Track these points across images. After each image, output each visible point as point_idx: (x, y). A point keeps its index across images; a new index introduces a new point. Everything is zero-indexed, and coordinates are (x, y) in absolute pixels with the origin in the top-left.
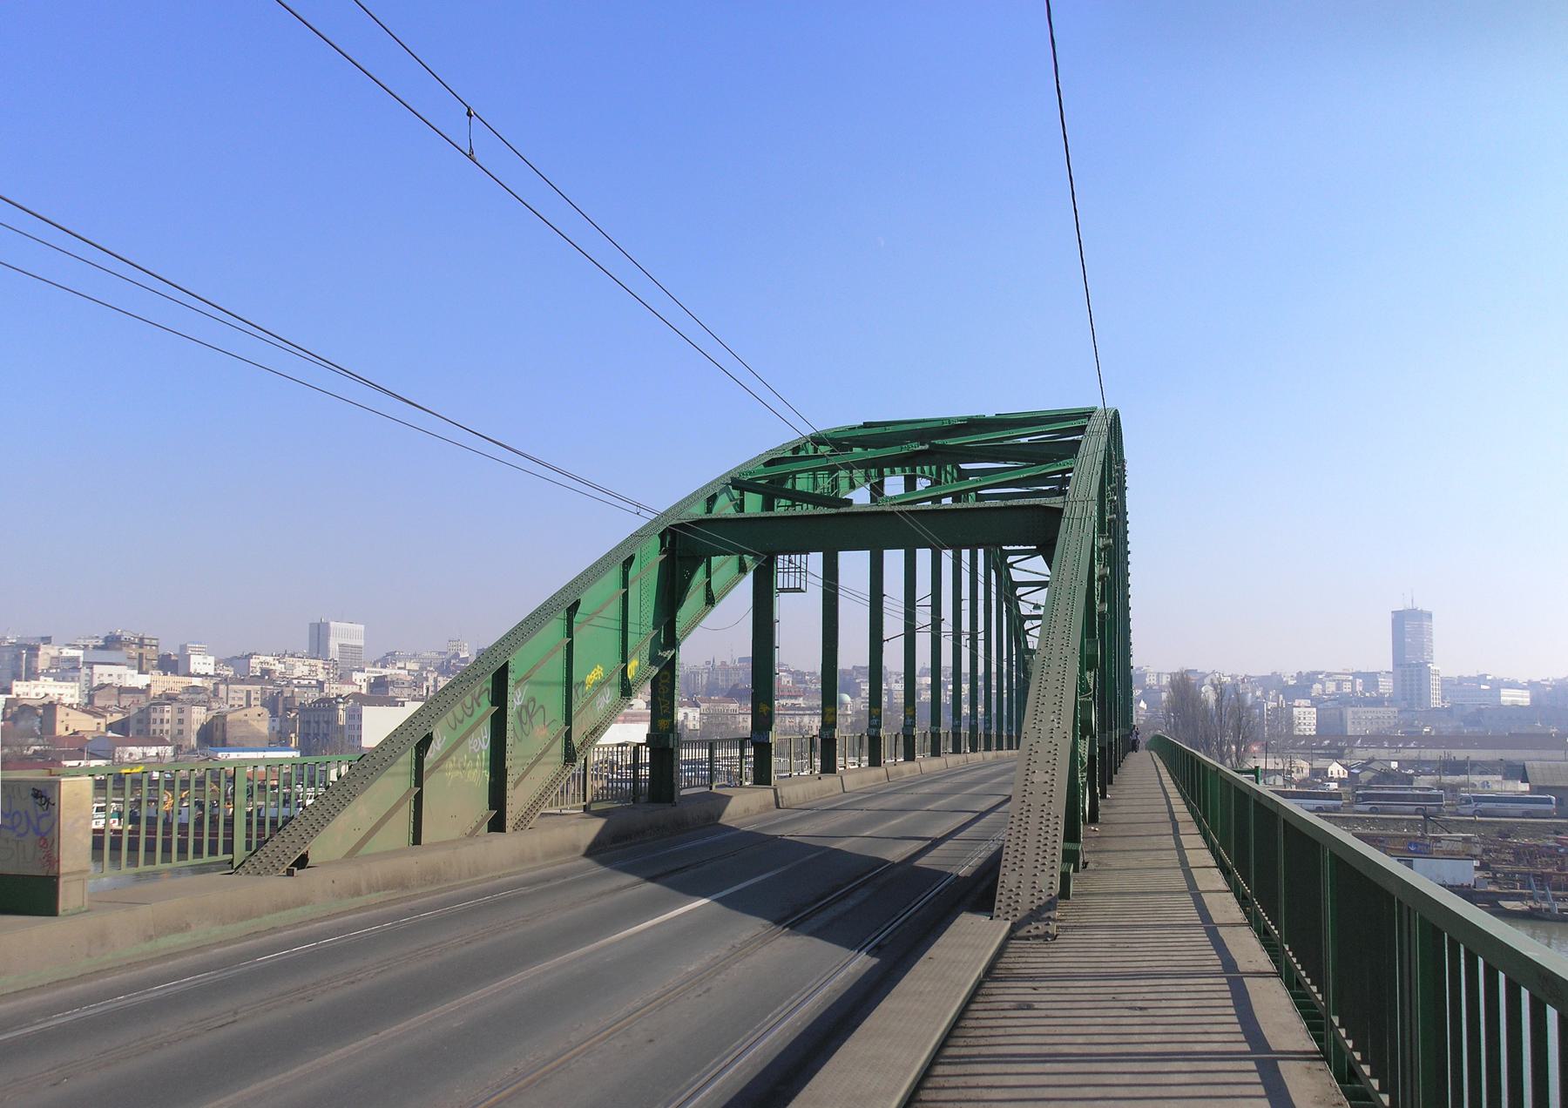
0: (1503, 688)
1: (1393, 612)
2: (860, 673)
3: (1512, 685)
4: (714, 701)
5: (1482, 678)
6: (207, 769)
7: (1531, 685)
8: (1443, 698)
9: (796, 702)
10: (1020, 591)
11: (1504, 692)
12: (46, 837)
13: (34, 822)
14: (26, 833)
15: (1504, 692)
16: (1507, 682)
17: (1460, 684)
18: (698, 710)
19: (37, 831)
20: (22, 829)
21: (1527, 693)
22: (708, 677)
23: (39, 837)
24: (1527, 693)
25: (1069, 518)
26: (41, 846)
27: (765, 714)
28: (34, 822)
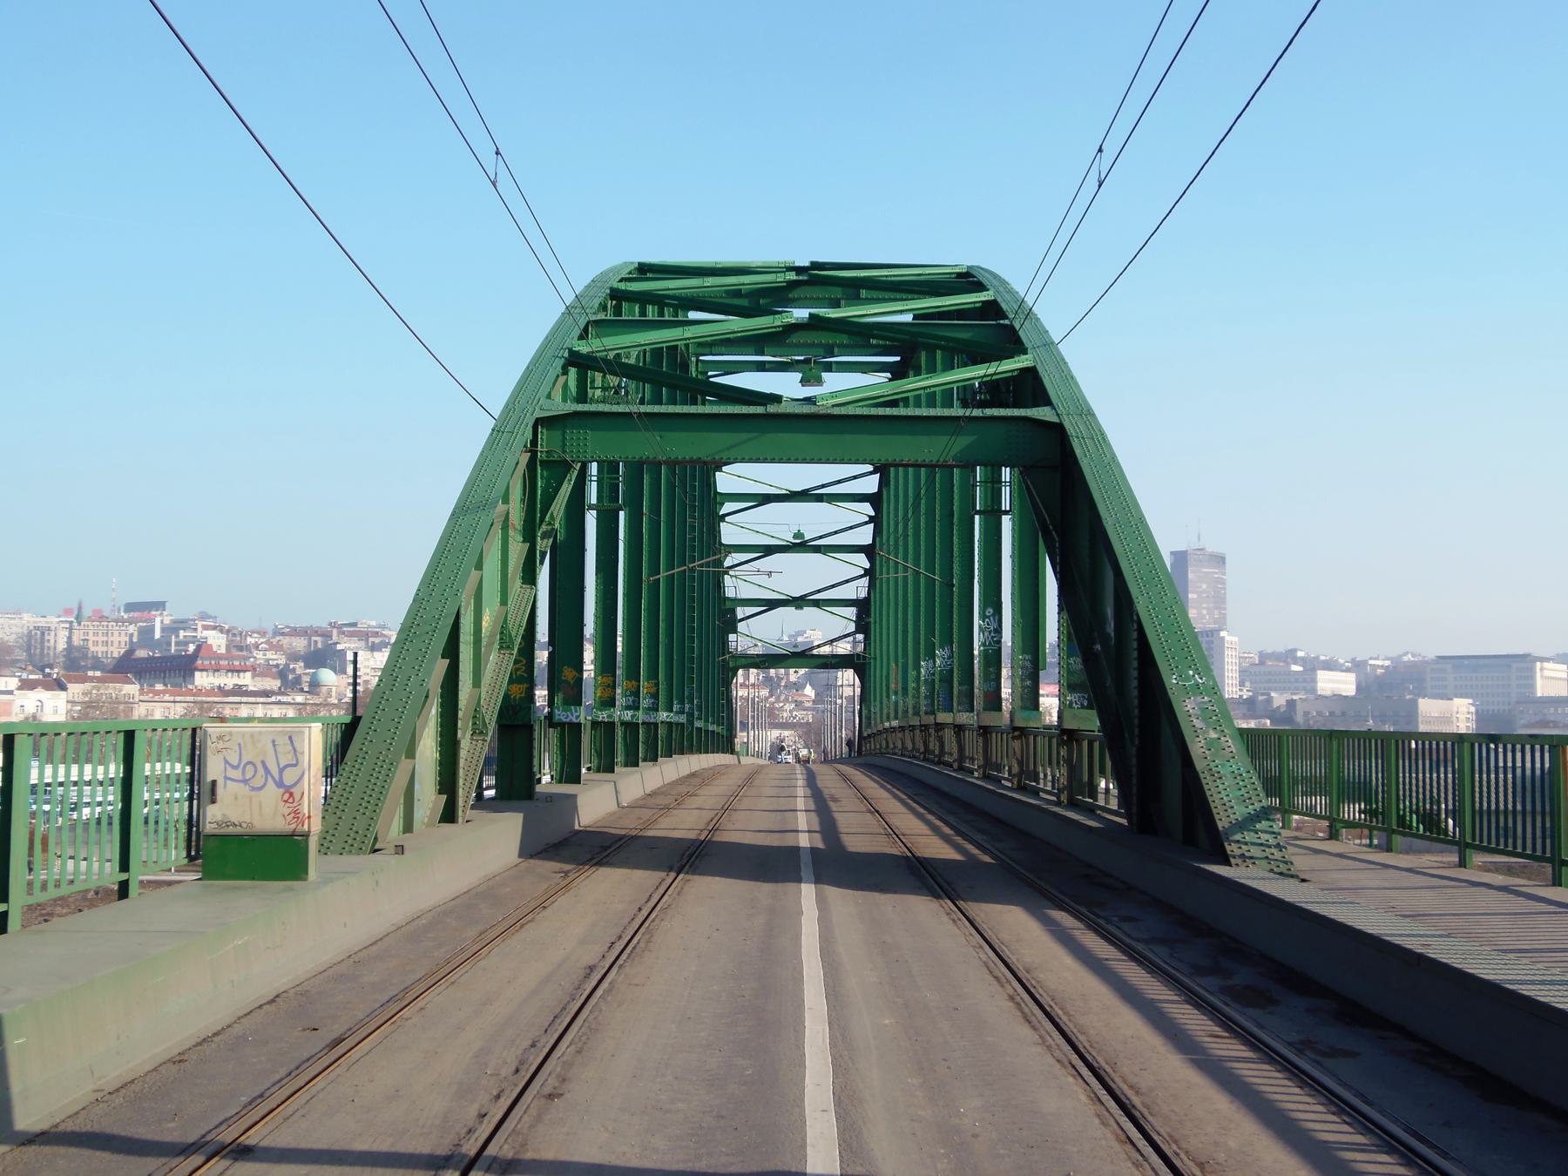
0: (1320, 669)
1: (1172, 553)
2: (343, 633)
3: (1330, 666)
4: (92, 679)
5: (1290, 656)
6: (69, 734)
7: (1357, 666)
8: (1242, 684)
9: (240, 682)
10: (728, 507)
11: (1322, 675)
12: (292, 790)
13: (275, 772)
14: (265, 784)
15: (1322, 675)
16: (1323, 661)
17: (1262, 663)
18: (63, 694)
19: (280, 784)
20: (258, 782)
21: (1352, 677)
22: (70, 638)
23: (282, 790)
24: (1352, 677)
25: (1078, 437)
26: (286, 801)
27: (572, 682)
28: (275, 772)
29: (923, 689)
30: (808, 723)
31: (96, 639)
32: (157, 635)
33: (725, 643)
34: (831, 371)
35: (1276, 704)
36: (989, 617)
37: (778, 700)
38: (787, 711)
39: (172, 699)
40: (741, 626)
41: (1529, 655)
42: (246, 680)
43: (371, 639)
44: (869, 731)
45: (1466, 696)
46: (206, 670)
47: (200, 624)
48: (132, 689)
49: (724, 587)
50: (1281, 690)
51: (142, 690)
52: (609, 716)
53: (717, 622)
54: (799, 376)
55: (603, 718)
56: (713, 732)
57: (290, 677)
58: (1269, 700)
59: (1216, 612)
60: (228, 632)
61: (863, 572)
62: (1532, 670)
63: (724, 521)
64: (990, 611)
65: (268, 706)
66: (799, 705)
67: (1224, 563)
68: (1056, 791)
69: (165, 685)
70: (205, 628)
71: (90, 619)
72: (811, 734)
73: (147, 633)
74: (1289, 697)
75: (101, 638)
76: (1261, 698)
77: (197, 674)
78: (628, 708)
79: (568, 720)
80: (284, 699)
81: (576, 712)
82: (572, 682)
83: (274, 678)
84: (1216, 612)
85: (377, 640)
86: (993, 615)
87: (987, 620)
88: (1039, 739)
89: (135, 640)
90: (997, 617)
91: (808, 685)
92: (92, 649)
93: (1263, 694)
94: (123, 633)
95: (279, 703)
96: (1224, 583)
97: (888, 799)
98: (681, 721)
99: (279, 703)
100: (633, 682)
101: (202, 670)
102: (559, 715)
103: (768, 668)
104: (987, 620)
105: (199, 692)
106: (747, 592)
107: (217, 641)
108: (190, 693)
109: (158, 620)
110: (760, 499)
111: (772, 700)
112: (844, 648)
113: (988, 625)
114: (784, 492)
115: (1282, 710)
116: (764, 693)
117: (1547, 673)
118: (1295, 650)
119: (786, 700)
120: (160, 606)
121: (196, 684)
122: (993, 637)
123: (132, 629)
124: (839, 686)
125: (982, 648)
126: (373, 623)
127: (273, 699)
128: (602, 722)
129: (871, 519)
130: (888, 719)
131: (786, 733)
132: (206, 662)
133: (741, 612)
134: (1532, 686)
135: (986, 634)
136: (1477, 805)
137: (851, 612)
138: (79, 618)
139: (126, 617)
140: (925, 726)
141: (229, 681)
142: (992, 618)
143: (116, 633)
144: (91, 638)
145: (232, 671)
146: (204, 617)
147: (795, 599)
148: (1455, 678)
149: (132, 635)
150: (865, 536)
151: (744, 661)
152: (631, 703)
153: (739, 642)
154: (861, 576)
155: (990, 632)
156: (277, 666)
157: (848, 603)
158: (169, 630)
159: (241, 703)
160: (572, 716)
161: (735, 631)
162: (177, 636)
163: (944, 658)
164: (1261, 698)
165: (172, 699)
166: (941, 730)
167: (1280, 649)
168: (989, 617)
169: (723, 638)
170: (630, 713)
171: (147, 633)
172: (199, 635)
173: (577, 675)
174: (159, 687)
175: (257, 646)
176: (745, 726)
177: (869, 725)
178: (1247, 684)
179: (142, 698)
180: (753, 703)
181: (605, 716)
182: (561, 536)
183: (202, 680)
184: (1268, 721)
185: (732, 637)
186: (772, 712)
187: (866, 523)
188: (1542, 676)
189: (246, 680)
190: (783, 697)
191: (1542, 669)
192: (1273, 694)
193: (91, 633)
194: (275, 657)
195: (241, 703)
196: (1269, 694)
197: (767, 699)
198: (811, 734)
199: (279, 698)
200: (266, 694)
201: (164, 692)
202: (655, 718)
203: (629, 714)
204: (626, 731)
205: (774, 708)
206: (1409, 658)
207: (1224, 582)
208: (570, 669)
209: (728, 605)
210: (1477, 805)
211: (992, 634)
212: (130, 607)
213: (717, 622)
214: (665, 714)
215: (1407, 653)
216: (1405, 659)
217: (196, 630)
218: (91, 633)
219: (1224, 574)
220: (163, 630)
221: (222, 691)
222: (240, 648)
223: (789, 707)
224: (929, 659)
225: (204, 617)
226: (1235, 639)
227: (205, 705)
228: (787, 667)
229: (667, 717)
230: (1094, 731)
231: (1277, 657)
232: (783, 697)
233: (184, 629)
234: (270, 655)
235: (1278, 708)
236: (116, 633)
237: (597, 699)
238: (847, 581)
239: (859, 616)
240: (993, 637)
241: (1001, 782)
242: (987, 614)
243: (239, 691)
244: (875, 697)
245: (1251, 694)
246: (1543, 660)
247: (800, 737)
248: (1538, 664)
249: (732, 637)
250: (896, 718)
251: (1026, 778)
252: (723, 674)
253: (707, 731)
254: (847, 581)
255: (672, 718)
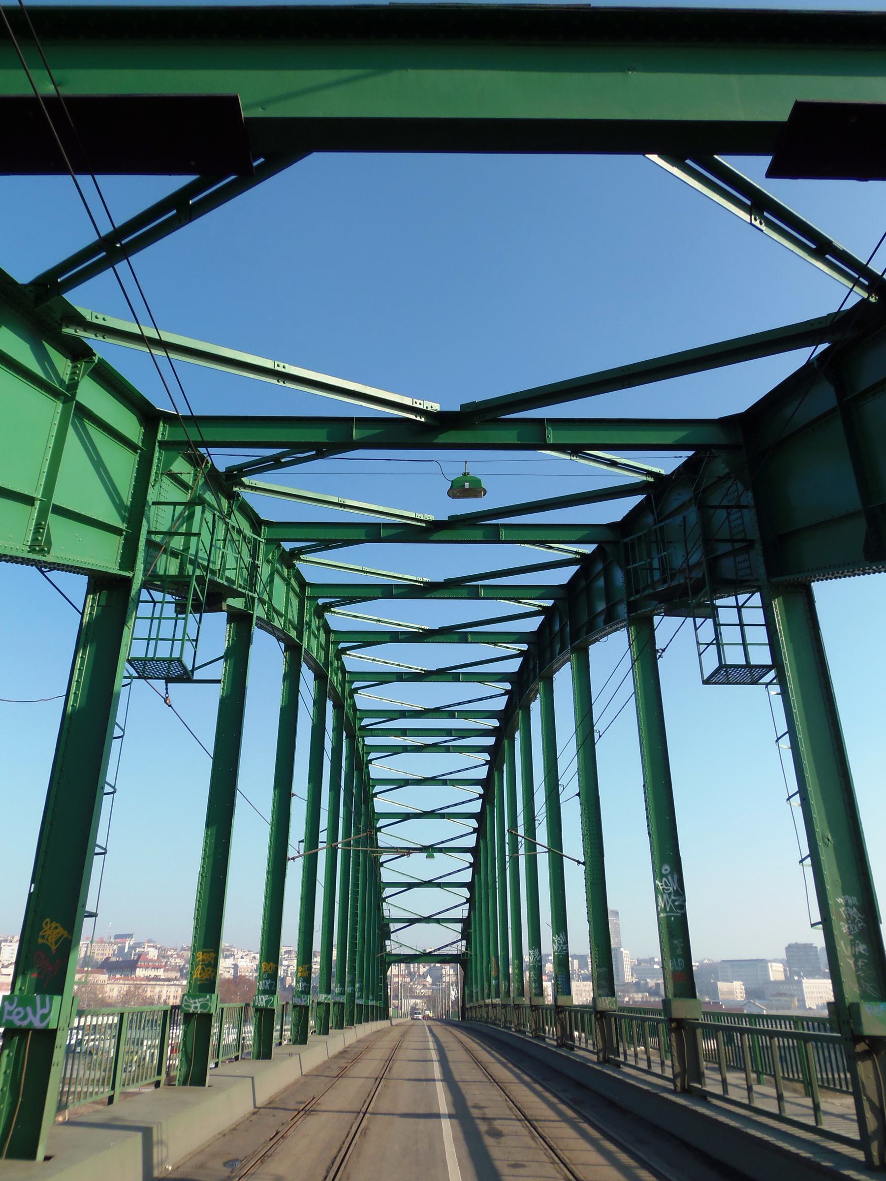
8: (632, 975)
9: (158, 974)
17: (639, 964)
22: (86, 952)
29: (527, 975)
30: (428, 996)
31: (98, 952)
32: (126, 950)
33: (383, 946)
34: (447, 785)
35: (650, 986)
36: (666, 876)
37: (414, 984)
38: (419, 989)
39: (123, 982)
40: (393, 936)
41: (764, 960)
42: (161, 973)
43: (225, 953)
44: (471, 1004)
45: (741, 980)
46: (142, 968)
47: (146, 945)
48: (103, 977)
49: (383, 910)
50: (652, 978)
51: (109, 978)
52: (204, 1006)
53: (377, 931)
54: (425, 855)
55: (196, 1008)
56: (373, 1006)
57: (185, 971)
58: (647, 983)
59: (616, 939)
60: (159, 948)
61: (465, 900)
62: (767, 967)
63: (383, 866)
64: (666, 869)
65: (169, 987)
66: (424, 986)
67: (618, 915)
68: (596, 1051)
69: (121, 975)
70: (149, 947)
71: (97, 942)
72: (431, 1001)
73: (121, 949)
74: (656, 982)
75: (100, 952)
76: (642, 982)
77: (138, 969)
78: (264, 992)
79: (25, 1024)
80: (177, 983)
81: (43, 1006)
82: (54, 948)
83: (177, 972)
84: (616, 939)
85: (228, 953)
86: (671, 873)
87: (664, 879)
88: (623, 1021)
89: (116, 952)
90: (676, 877)
91: (428, 976)
92: (96, 957)
93: (643, 980)
94: (111, 949)
95: (175, 985)
96: (619, 925)
97: (494, 1063)
98: (341, 1001)
99: (175, 985)
100: (272, 964)
101: (140, 968)
102: (10, 1013)
103: (409, 963)
104: (664, 879)
105: (137, 979)
106: (395, 913)
107: (153, 954)
108: (132, 979)
109: (127, 943)
110: (404, 816)
111: (412, 983)
112: (453, 950)
113: (666, 885)
114: (419, 812)
115: (654, 988)
116: (408, 980)
117: (774, 968)
118: (654, 958)
119: (418, 984)
120: (130, 936)
121: (137, 975)
122: (673, 901)
123: (115, 947)
124: (78, 1053)
125: (662, 915)
126: (227, 945)
127: (172, 983)
128: (193, 1014)
129: (471, 865)
130: (489, 997)
131: (418, 1001)
132: (143, 964)
133: (393, 926)
134: (768, 975)
135: (665, 896)
136: (761, 1044)
137: (459, 927)
138: (92, 942)
139: (113, 941)
140: (535, 1006)
141: (152, 973)
142: (670, 878)
143: (108, 949)
144: (96, 952)
145: (155, 968)
146: (150, 941)
147: (425, 918)
148: (732, 971)
149: (115, 950)
150: (467, 876)
151: (395, 958)
152: (267, 987)
153: (392, 947)
154: (465, 903)
155: (670, 894)
156: (180, 966)
157: (456, 920)
158: (132, 948)
159: (156, 985)
160: (35, 1013)
161: (389, 939)
162: (135, 951)
163: (560, 944)
164: (642, 982)
165: (123, 982)
166: (561, 1012)
167: (646, 957)
168: (666, 876)
169: (382, 943)
170: (265, 998)
171: (121, 949)
172: (145, 950)
173: (66, 934)
174: (118, 976)
175: (172, 956)
176: (396, 997)
177: (471, 1000)
178: (635, 975)
179: (109, 982)
180: (401, 984)
181: (198, 1005)
182: (75, 701)
183: (140, 972)
184: (647, 994)
185: (387, 942)
186: (411, 990)
187: (468, 868)
188: (772, 970)
189: (161, 973)
190: (416, 982)
191: (771, 967)
192: (648, 980)
193: (96, 949)
194: (179, 961)
195: (156, 985)
196: (646, 980)
197: (409, 983)
198: (431, 1001)
199: (175, 982)
200: (169, 980)
201: (120, 979)
202: (305, 1001)
203: (264, 1000)
204: (260, 1018)
205: (413, 988)
206: (706, 961)
207: (618, 924)
208: (54, 924)
209: (385, 922)
210: (761, 1044)
211: (673, 897)
212: (117, 937)
213: (377, 931)
214: (324, 996)
215: (705, 959)
216: (705, 962)
217: (144, 948)
218: (96, 949)
219: (619, 920)
220: (129, 948)
221: (148, 979)
222: (164, 957)
223: (419, 987)
224: (535, 948)
225: (150, 941)
226: (627, 952)
227: (138, 986)
228: (419, 963)
229: (325, 998)
230: (698, 1020)
231: (645, 961)
232: (416, 982)
233: (139, 947)
234: (178, 960)
235: (651, 987)
236: (108, 949)
237: (193, 982)
238: (456, 907)
239: (463, 929)
240: (673, 901)
241: (619, 1067)
242: (664, 872)
243: (156, 978)
244: (476, 983)
245: (637, 980)
246: (771, 961)
247: (425, 1003)
248: (769, 964)
249: (387, 942)
250: (498, 996)
251: (566, 1040)
252: (381, 966)
253: (368, 1006)
254: (456, 907)
255: (329, 999)
